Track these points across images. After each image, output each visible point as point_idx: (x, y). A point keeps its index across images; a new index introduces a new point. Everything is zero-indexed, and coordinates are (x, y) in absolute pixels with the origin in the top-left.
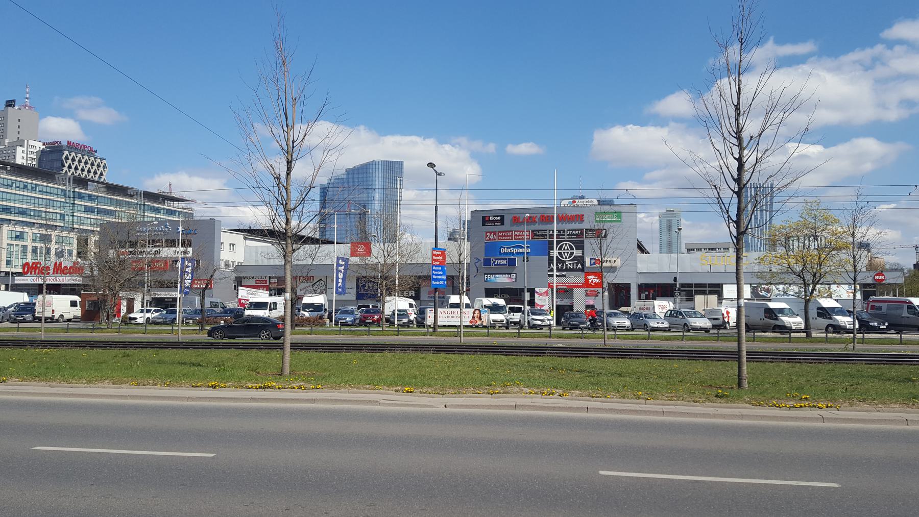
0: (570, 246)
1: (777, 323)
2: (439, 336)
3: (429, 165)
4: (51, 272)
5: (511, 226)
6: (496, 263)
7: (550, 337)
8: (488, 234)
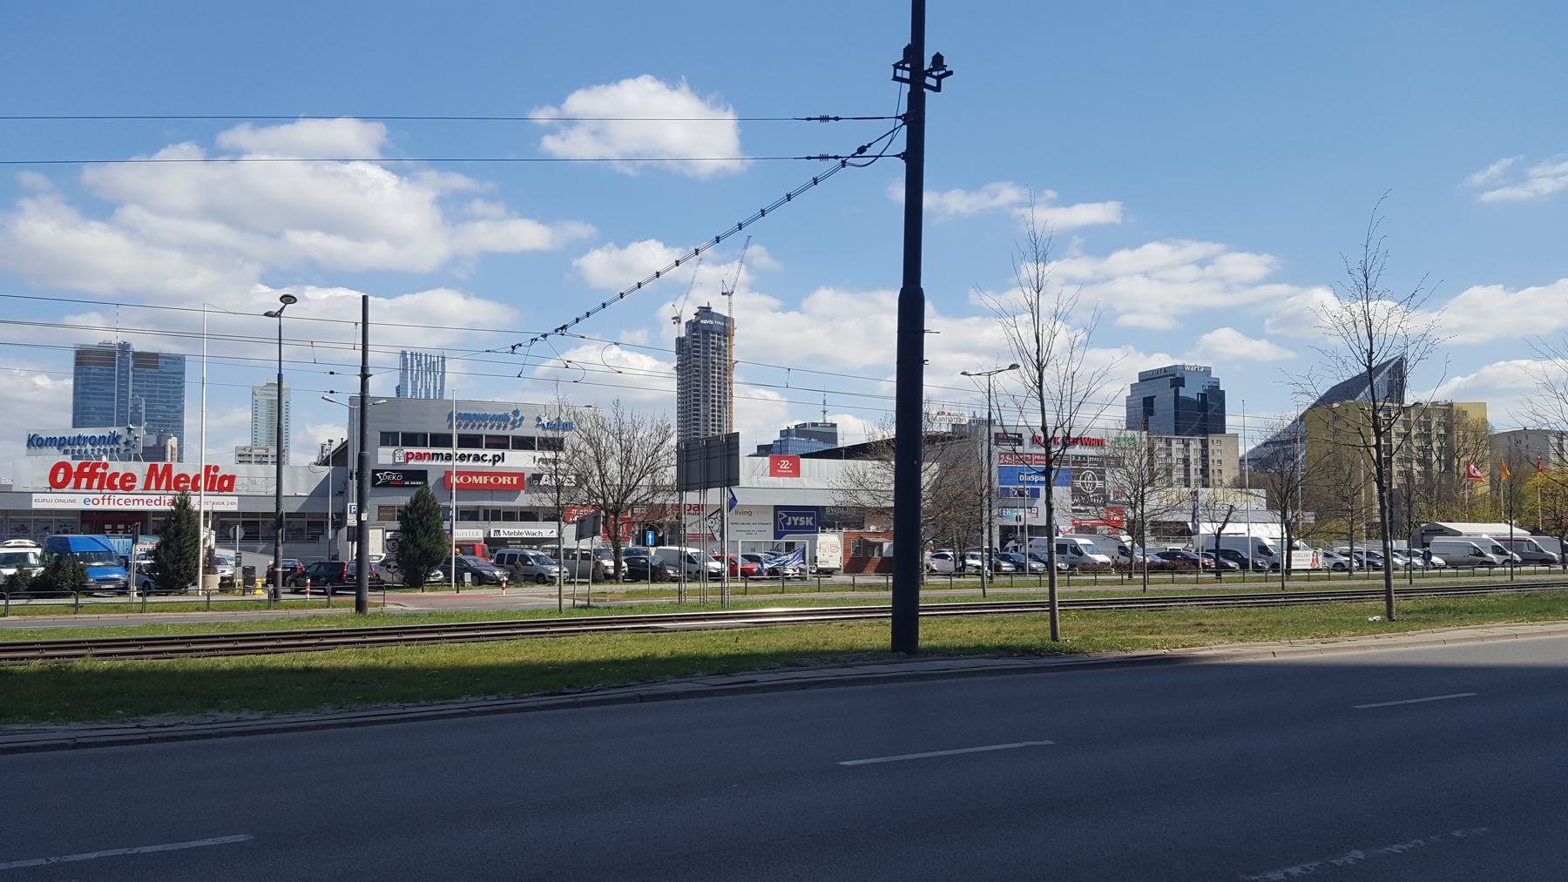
0: (1093, 476)
1: (1485, 559)
2: (997, 587)
3: (284, 299)
4: (139, 484)
5: (1031, 447)
6: (789, 524)
7: (208, 609)
8: (1003, 456)
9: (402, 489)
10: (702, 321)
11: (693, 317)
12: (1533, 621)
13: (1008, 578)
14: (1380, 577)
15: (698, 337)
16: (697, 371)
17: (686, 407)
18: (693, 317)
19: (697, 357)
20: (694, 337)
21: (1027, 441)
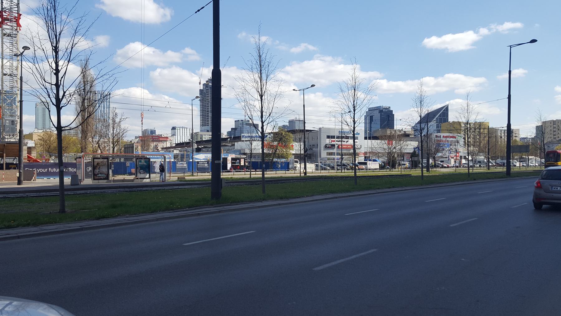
9: (331, 149)
10: (209, 84)
11: (205, 82)
12: (34, 226)
13: (244, 173)
14: (466, 169)
15: (208, 89)
16: (208, 101)
17: (204, 114)
18: (205, 82)
19: (208, 96)
20: (207, 89)
21: (442, 137)
